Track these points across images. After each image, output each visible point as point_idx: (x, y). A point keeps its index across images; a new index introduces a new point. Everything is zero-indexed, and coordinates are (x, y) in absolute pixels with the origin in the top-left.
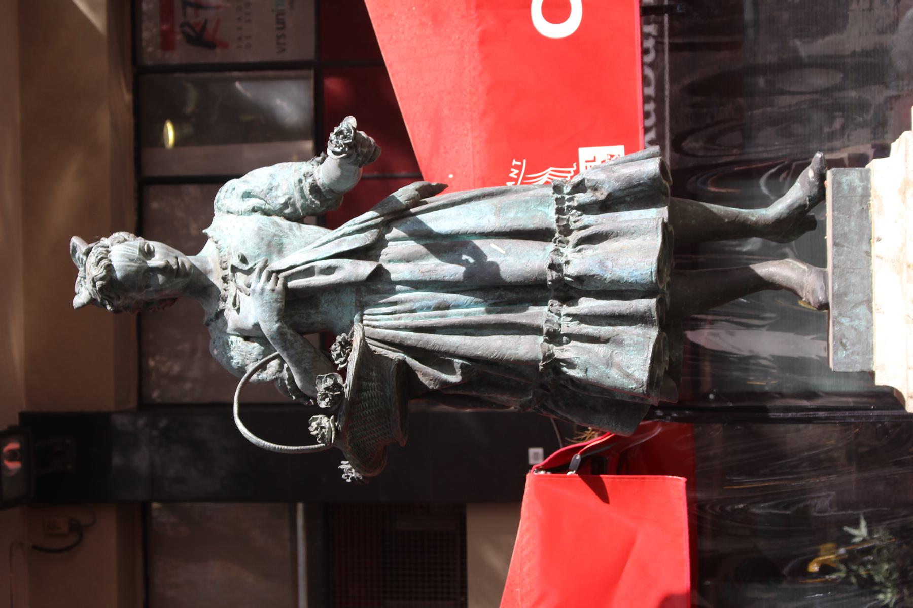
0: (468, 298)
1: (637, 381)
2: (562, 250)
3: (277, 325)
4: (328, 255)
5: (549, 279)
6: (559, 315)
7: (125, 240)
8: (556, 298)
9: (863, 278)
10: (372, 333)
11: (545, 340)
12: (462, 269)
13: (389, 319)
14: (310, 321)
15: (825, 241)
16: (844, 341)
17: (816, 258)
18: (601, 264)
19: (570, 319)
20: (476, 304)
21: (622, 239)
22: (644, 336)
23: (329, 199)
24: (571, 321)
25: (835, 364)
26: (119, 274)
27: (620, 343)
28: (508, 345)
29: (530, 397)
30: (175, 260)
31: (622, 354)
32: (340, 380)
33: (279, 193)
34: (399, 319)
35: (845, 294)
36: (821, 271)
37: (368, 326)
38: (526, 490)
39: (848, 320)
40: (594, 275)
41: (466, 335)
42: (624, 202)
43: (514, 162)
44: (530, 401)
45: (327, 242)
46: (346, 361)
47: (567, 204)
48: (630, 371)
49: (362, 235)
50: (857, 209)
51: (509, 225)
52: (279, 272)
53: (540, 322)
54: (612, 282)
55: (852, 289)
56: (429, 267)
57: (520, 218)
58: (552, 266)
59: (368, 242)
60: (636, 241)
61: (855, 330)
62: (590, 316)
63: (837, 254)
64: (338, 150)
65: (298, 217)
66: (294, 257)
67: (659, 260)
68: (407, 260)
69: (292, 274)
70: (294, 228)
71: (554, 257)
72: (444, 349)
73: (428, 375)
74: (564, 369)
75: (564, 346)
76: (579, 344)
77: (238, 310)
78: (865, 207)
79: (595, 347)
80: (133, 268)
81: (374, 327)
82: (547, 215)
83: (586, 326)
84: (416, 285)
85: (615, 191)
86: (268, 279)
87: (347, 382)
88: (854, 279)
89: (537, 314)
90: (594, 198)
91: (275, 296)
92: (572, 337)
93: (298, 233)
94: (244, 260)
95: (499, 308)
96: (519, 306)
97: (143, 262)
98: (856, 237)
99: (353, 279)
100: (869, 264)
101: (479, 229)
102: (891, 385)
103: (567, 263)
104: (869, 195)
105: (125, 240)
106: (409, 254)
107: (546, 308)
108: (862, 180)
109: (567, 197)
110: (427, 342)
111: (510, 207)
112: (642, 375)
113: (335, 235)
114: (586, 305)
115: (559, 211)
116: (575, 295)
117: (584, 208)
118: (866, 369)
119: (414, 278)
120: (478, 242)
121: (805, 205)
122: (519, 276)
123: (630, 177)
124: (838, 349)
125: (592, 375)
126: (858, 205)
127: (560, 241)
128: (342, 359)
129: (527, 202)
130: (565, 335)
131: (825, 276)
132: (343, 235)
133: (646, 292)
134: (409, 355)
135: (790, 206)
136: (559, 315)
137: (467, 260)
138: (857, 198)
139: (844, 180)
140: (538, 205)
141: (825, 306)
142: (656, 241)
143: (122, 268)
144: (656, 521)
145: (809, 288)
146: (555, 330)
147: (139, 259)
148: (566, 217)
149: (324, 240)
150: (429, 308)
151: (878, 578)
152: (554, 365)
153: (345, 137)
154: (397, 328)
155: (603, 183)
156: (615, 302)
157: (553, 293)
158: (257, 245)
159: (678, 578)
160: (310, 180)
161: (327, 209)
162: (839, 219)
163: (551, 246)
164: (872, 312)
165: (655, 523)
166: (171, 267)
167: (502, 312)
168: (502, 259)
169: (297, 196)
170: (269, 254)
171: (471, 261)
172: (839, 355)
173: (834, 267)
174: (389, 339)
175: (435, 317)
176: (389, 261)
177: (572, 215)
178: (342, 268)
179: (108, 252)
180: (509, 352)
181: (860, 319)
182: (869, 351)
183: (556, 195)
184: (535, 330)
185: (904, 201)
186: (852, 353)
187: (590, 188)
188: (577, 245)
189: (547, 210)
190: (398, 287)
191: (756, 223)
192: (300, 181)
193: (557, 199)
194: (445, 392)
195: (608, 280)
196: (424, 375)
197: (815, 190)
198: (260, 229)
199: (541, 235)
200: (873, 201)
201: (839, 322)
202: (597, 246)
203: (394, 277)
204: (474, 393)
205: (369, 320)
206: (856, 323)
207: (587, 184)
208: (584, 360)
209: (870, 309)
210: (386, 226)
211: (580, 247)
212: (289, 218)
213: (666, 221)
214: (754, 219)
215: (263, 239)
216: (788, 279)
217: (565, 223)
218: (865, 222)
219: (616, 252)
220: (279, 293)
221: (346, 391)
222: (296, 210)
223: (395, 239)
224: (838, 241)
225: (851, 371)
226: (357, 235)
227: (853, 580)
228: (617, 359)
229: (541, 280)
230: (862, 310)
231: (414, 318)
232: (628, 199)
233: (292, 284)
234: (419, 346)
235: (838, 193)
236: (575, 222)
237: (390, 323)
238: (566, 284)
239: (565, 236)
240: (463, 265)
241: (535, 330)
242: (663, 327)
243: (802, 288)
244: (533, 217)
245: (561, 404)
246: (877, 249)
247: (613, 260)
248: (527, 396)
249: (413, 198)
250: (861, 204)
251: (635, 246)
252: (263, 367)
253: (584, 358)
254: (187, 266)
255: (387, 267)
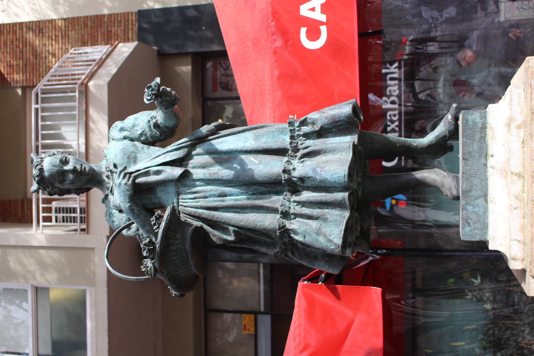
0: (237, 190)
1: (335, 244)
2: (292, 161)
3: (129, 204)
4: (158, 164)
5: (283, 179)
6: (289, 201)
7: (54, 154)
8: (289, 191)
9: (482, 180)
10: (184, 210)
11: (281, 217)
12: (233, 172)
13: (192, 202)
14: (152, 202)
15: (458, 158)
16: (469, 221)
17: (453, 169)
18: (314, 170)
19: (296, 204)
20: (242, 194)
21: (328, 155)
22: (340, 216)
23: (166, 132)
24: (297, 205)
25: (463, 236)
26: (46, 174)
27: (325, 220)
28: (260, 219)
29: (278, 249)
30: (80, 166)
31: (326, 227)
32: (154, 240)
33: (138, 128)
34: (198, 202)
35: (470, 191)
36: (455, 176)
37: (182, 206)
38: (298, 291)
39: (472, 207)
40: (310, 177)
41: (235, 212)
42: (332, 132)
43: (290, 116)
44: (278, 252)
45: (158, 156)
46: (158, 227)
47: (297, 133)
48: (331, 238)
49: (178, 152)
50: (478, 136)
51: (262, 146)
52: (131, 173)
53: (277, 205)
54: (321, 181)
55: (474, 187)
56: (214, 171)
57: (269, 142)
58: (284, 171)
59: (181, 156)
60: (337, 156)
61: (476, 214)
62: (307, 202)
63: (465, 165)
64: (149, 98)
65: (151, 142)
66: (140, 165)
67: (350, 168)
68: (203, 167)
69: (139, 175)
70: (145, 148)
71: (287, 166)
72: (223, 221)
73: (216, 235)
74: (292, 235)
75: (292, 221)
76: (301, 220)
77: (113, 194)
78: (483, 135)
79: (310, 222)
80: (55, 171)
81: (185, 206)
82: (285, 140)
83: (306, 209)
84: (208, 182)
85: (324, 125)
86: (124, 177)
87: (158, 241)
88: (476, 181)
89: (276, 201)
90: (313, 129)
91: (127, 187)
92: (296, 215)
93: (146, 151)
94: (115, 166)
95: (255, 197)
96: (268, 196)
97: (61, 167)
98: (477, 154)
99: (171, 178)
100: (486, 172)
101: (245, 149)
102: (499, 250)
103: (294, 169)
104: (486, 128)
105: (54, 154)
106: (204, 164)
107: (281, 197)
108: (481, 118)
109: (297, 129)
110: (213, 216)
111: (263, 135)
112: (338, 240)
113: (163, 152)
114: (306, 195)
115: (292, 137)
116: (301, 189)
117: (307, 136)
118: (483, 239)
119: (206, 178)
120: (243, 157)
121: (446, 136)
122: (265, 177)
123: (334, 116)
124: (465, 226)
125: (308, 240)
126: (479, 134)
127: (291, 156)
128: (156, 227)
129: (273, 132)
130: (293, 214)
131: (457, 179)
132: (167, 152)
133: (343, 188)
134: (205, 223)
135: (437, 137)
136: (289, 201)
137: (236, 167)
138: (478, 130)
139: (470, 118)
140: (279, 134)
141: (457, 198)
142: (349, 156)
143: (48, 170)
144: (364, 313)
145: (447, 186)
146: (286, 211)
147: (58, 165)
148: (296, 141)
149: (160, 153)
150: (214, 196)
151: (484, 299)
152: (285, 232)
153: (153, 90)
154: (201, 208)
155: (317, 120)
156: (323, 194)
157: (287, 188)
158: (122, 157)
159: (378, 342)
160: (154, 121)
161: (160, 137)
162: (466, 142)
163: (286, 159)
164: (487, 203)
165: (364, 313)
166: (77, 170)
167: (256, 199)
168: (256, 166)
169: (147, 130)
170: (129, 163)
171: (239, 167)
172: (466, 230)
173: (463, 173)
174: (192, 213)
175: (218, 201)
176: (193, 168)
177: (300, 140)
178: (165, 171)
179: (42, 161)
180: (259, 224)
181: (479, 207)
182: (485, 227)
183: (290, 128)
184: (274, 210)
185: (509, 131)
186: (474, 229)
187: (310, 123)
188: (301, 158)
189: (285, 137)
190: (198, 183)
191: (416, 147)
192: (149, 121)
193: (291, 130)
194: (226, 245)
195: (318, 180)
196: (214, 235)
197: (452, 127)
198: (124, 148)
199: (280, 152)
200: (489, 132)
201: (466, 209)
202: (313, 159)
203: (195, 177)
204: (245, 246)
205: (183, 202)
206: (476, 209)
207: (309, 121)
208: (302, 230)
209: (486, 201)
210: (192, 146)
211: (302, 160)
212: (144, 143)
213: (356, 143)
214: (415, 144)
215: (125, 154)
216: (435, 180)
217: (295, 145)
218: (483, 145)
219: (323, 163)
220: (129, 186)
221: (157, 246)
222: (147, 138)
223: (198, 154)
224: (465, 157)
225: (473, 240)
226: (175, 152)
227: (475, 299)
228: (324, 230)
229: (279, 178)
230: (481, 201)
231: (206, 202)
232: (334, 130)
233: (138, 180)
234: (209, 218)
235: (466, 126)
236: (301, 144)
237: (193, 204)
238: (294, 183)
239: (296, 153)
240: (233, 170)
241: (274, 210)
242: (353, 209)
243: (443, 186)
244: (276, 141)
245: (296, 254)
246: (491, 162)
247: (321, 168)
248: (276, 248)
249: (211, 131)
250: (481, 134)
251: (335, 161)
252: (128, 227)
253: (303, 229)
254: (87, 169)
255: (192, 171)
